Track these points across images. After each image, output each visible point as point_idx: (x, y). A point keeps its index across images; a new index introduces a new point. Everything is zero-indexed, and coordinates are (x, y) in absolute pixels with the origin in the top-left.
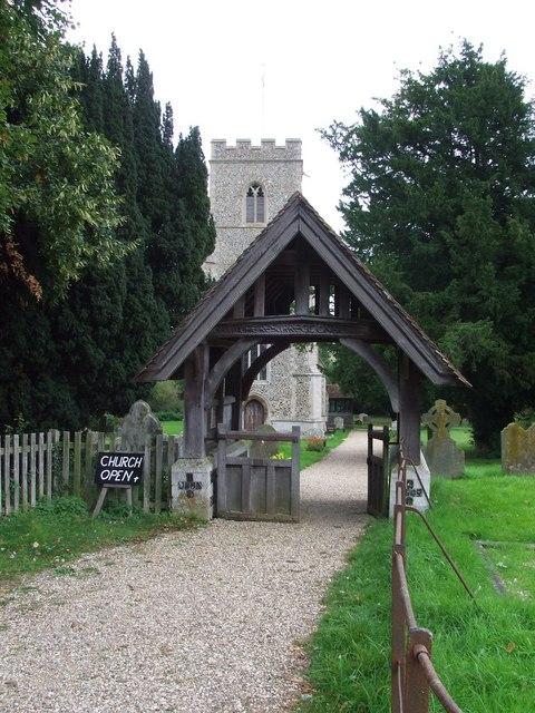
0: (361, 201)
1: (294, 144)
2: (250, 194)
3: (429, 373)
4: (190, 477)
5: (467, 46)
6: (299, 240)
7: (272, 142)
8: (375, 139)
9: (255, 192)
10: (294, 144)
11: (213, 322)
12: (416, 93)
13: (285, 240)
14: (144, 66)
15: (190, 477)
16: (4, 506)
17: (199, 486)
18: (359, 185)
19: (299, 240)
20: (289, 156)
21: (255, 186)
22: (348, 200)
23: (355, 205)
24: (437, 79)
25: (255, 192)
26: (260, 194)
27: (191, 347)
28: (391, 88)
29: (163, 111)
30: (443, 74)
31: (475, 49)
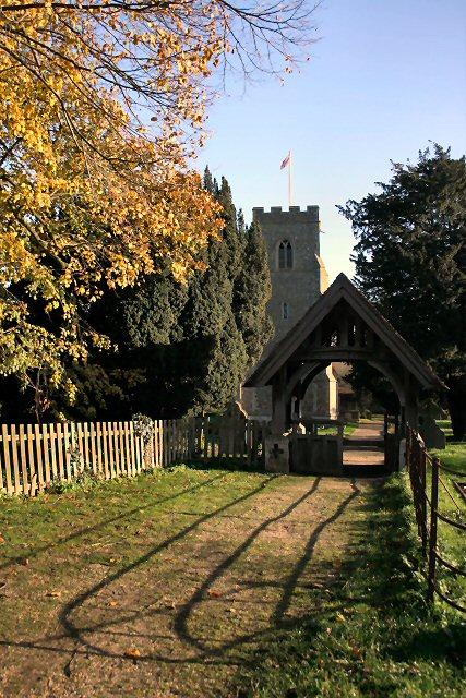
0: (365, 254)
1: (313, 210)
2: (281, 247)
3: (423, 382)
4: (276, 446)
5: (438, 148)
6: (343, 302)
7: (298, 208)
8: (376, 213)
9: (285, 246)
10: (313, 210)
11: (291, 352)
12: (403, 178)
13: (334, 302)
14: (225, 183)
15: (276, 446)
16: (5, 485)
17: (282, 451)
18: (365, 243)
19: (343, 302)
20: (305, 222)
21: (285, 241)
22: (356, 254)
23: (361, 256)
24: (419, 172)
25: (285, 246)
26: (289, 247)
27: (276, 369)
28: (388, 177)
29: (238, 210)
30: (425, 167)
31: (445, 150)
